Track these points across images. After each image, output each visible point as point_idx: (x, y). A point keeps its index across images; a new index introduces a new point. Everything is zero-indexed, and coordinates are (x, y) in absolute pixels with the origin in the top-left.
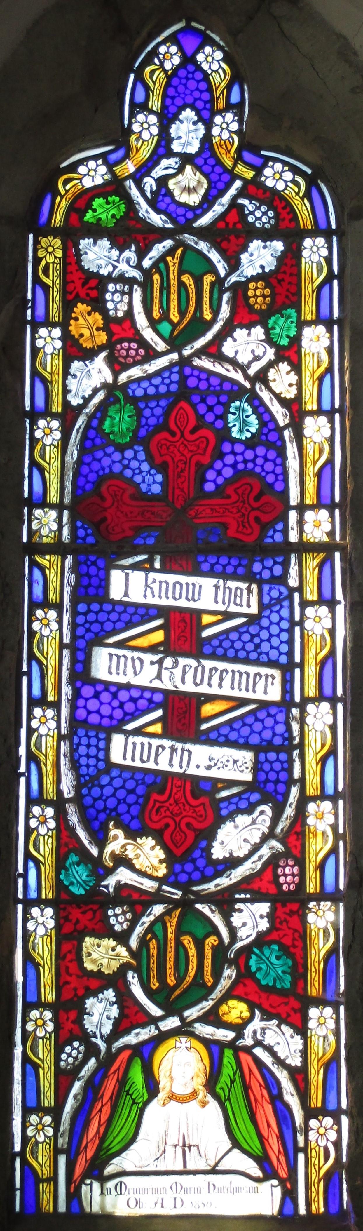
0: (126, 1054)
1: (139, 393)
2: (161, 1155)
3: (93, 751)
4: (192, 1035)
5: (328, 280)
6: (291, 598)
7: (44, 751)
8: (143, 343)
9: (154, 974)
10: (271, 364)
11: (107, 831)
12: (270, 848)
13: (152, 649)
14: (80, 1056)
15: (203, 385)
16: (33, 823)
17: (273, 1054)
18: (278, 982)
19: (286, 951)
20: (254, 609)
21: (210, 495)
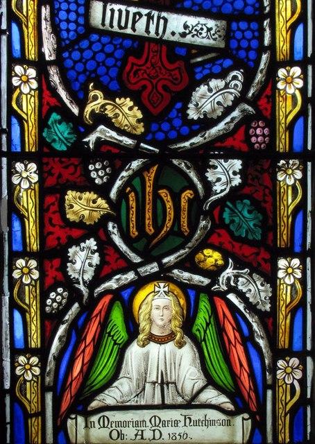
0: (107, 299)
2: (141, 392)
4: (170, 280)
7: (25, 13)
11: (87, 91)
12: (242, 111)
14: (64, 301)
18: (250, 233)
19: (256, 206)
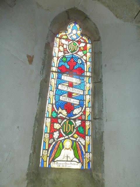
0: (60, 141)
1: (67, 57)
3: (58, 98)
4: (70, 139)
5: (90, 48)
6: (85, 82)
8: (68, 51)
9: (64, 129)
10: (83, 56)
13: (67, 86)
15: (75, 57)
16: (49, 106)
17: (81, 143)
20: (80, 83)
21: (75, 69)
